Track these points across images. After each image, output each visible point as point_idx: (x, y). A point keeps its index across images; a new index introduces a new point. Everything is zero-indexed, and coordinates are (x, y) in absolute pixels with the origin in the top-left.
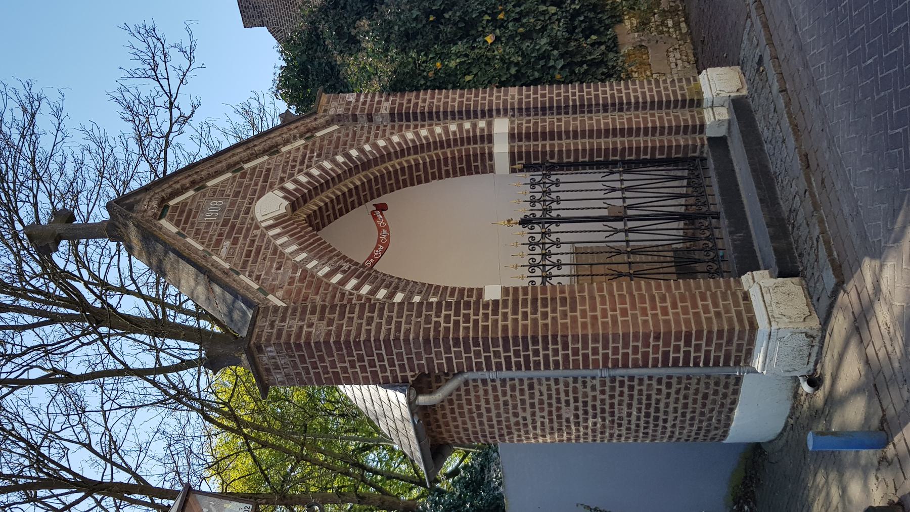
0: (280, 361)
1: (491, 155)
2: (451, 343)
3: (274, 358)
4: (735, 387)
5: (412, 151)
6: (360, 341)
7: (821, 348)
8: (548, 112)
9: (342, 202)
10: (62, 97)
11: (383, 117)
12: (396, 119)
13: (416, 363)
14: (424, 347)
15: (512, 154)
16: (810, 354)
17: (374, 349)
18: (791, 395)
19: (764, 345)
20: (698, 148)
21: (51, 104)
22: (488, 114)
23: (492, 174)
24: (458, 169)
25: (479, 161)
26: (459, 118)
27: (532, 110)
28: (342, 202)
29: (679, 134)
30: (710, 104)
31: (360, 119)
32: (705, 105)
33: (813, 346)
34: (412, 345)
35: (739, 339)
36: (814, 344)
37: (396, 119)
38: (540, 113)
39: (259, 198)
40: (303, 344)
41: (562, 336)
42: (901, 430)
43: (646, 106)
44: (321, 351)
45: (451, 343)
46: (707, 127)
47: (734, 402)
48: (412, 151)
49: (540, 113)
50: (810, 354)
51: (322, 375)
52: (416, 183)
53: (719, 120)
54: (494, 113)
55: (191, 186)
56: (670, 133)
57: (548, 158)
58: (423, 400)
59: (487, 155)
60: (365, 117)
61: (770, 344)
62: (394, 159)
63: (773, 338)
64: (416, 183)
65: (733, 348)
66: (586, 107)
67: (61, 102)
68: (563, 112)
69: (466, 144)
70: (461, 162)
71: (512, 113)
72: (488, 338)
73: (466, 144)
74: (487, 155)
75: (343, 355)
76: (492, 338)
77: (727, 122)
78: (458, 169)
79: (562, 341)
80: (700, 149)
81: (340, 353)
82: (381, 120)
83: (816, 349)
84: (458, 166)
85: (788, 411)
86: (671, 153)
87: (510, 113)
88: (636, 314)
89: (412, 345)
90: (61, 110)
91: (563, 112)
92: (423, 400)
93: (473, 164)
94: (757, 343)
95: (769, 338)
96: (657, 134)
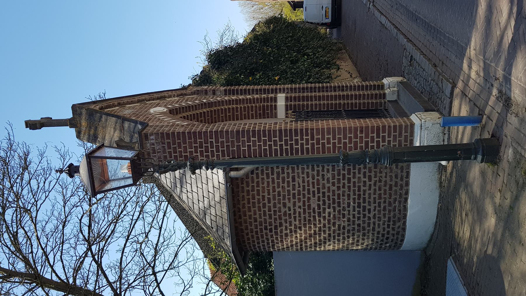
0: (157, 147)
1: (276, 106)
2: (251, 134)
3: (153, 144)
4: (407, 180)
5: (235, 103)
6: (202, 132)
7: (449, 134)
8: (305, 91)
9: (196, 118)
10: (46, 146)
11: (221, 92)
12: (228, 93)
13: (231, 149)
14: (236, 137)
15: (286, 106)
16: (444, 140)
17: (209, 138)
18: (438, 185)
19: (419, 134)
20: (383, 104)
21: (40, 150)
22: (275, 91)
23: (276, 118)
24: (258, 114)
25: (269, 110)
26: (260, 94)
27: (297, 89)
28: (196, 118)
29: (373, 99)
30: (388, 86)
31: (209, 93)
32: (385, 88)
33: (445, 134)
34: (230, 136)
35: (405, 132)
36: (445, 132)
37: (228, 93)
38: (302, 91)
39: (153, 108)
40: (170, 133)
41: (311, 129)
42: (488, 104)
43: (356, 89)
44: (180, 140)
45: (251, 134)
46: (387, 94)
47: (407, 193)
48: (235, 103)
49: (302, 91)
50: (444, 140)
51: (178, 158)
52: (235, 120)
53: (393, 91)
54: (278, 91)
55: (118, 105)
56: (368, 99)
57: (305, 108)
58: (233, 174)
59: (273, 107)
60: (211, 92)
61: (422, 133)
62: (225, 105)
63: (423, 128)
64: (235, 120)
65: (403, 138)
66: (325, 88)
67: (45, 148)
68: (313, 91)
69: (263, 102)
70: (260, 110)
71: (287, 91)
72: (271, 130)
73: (263, 102)
74: (273, 107)
75: (191, 142)
76: (273, 130)
77: (397, 91)
78: (258, 114)
79: (310, 133)
80: (384, 105)
81: (190, 140)
82: (219, 94)
83: (446, 136)
84: (258, 112)
85: (438, 199)
86: (369, 107)
87: (286, 91)
88: (350, 168)
89: (230, 136)
90: (44, 153)
91: (313, 91)
92: (233, 174)
93: (266, 112)
94: (415, 135)
95: (421, 128)
96: (362, 99)
